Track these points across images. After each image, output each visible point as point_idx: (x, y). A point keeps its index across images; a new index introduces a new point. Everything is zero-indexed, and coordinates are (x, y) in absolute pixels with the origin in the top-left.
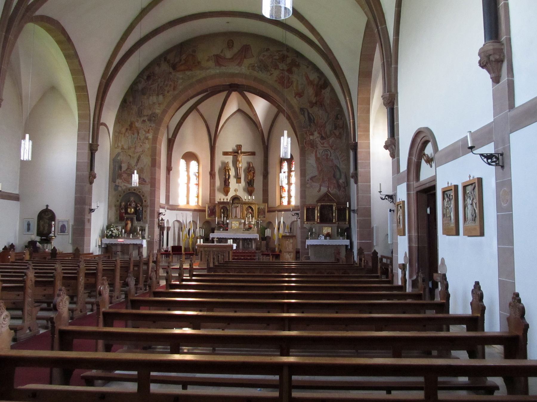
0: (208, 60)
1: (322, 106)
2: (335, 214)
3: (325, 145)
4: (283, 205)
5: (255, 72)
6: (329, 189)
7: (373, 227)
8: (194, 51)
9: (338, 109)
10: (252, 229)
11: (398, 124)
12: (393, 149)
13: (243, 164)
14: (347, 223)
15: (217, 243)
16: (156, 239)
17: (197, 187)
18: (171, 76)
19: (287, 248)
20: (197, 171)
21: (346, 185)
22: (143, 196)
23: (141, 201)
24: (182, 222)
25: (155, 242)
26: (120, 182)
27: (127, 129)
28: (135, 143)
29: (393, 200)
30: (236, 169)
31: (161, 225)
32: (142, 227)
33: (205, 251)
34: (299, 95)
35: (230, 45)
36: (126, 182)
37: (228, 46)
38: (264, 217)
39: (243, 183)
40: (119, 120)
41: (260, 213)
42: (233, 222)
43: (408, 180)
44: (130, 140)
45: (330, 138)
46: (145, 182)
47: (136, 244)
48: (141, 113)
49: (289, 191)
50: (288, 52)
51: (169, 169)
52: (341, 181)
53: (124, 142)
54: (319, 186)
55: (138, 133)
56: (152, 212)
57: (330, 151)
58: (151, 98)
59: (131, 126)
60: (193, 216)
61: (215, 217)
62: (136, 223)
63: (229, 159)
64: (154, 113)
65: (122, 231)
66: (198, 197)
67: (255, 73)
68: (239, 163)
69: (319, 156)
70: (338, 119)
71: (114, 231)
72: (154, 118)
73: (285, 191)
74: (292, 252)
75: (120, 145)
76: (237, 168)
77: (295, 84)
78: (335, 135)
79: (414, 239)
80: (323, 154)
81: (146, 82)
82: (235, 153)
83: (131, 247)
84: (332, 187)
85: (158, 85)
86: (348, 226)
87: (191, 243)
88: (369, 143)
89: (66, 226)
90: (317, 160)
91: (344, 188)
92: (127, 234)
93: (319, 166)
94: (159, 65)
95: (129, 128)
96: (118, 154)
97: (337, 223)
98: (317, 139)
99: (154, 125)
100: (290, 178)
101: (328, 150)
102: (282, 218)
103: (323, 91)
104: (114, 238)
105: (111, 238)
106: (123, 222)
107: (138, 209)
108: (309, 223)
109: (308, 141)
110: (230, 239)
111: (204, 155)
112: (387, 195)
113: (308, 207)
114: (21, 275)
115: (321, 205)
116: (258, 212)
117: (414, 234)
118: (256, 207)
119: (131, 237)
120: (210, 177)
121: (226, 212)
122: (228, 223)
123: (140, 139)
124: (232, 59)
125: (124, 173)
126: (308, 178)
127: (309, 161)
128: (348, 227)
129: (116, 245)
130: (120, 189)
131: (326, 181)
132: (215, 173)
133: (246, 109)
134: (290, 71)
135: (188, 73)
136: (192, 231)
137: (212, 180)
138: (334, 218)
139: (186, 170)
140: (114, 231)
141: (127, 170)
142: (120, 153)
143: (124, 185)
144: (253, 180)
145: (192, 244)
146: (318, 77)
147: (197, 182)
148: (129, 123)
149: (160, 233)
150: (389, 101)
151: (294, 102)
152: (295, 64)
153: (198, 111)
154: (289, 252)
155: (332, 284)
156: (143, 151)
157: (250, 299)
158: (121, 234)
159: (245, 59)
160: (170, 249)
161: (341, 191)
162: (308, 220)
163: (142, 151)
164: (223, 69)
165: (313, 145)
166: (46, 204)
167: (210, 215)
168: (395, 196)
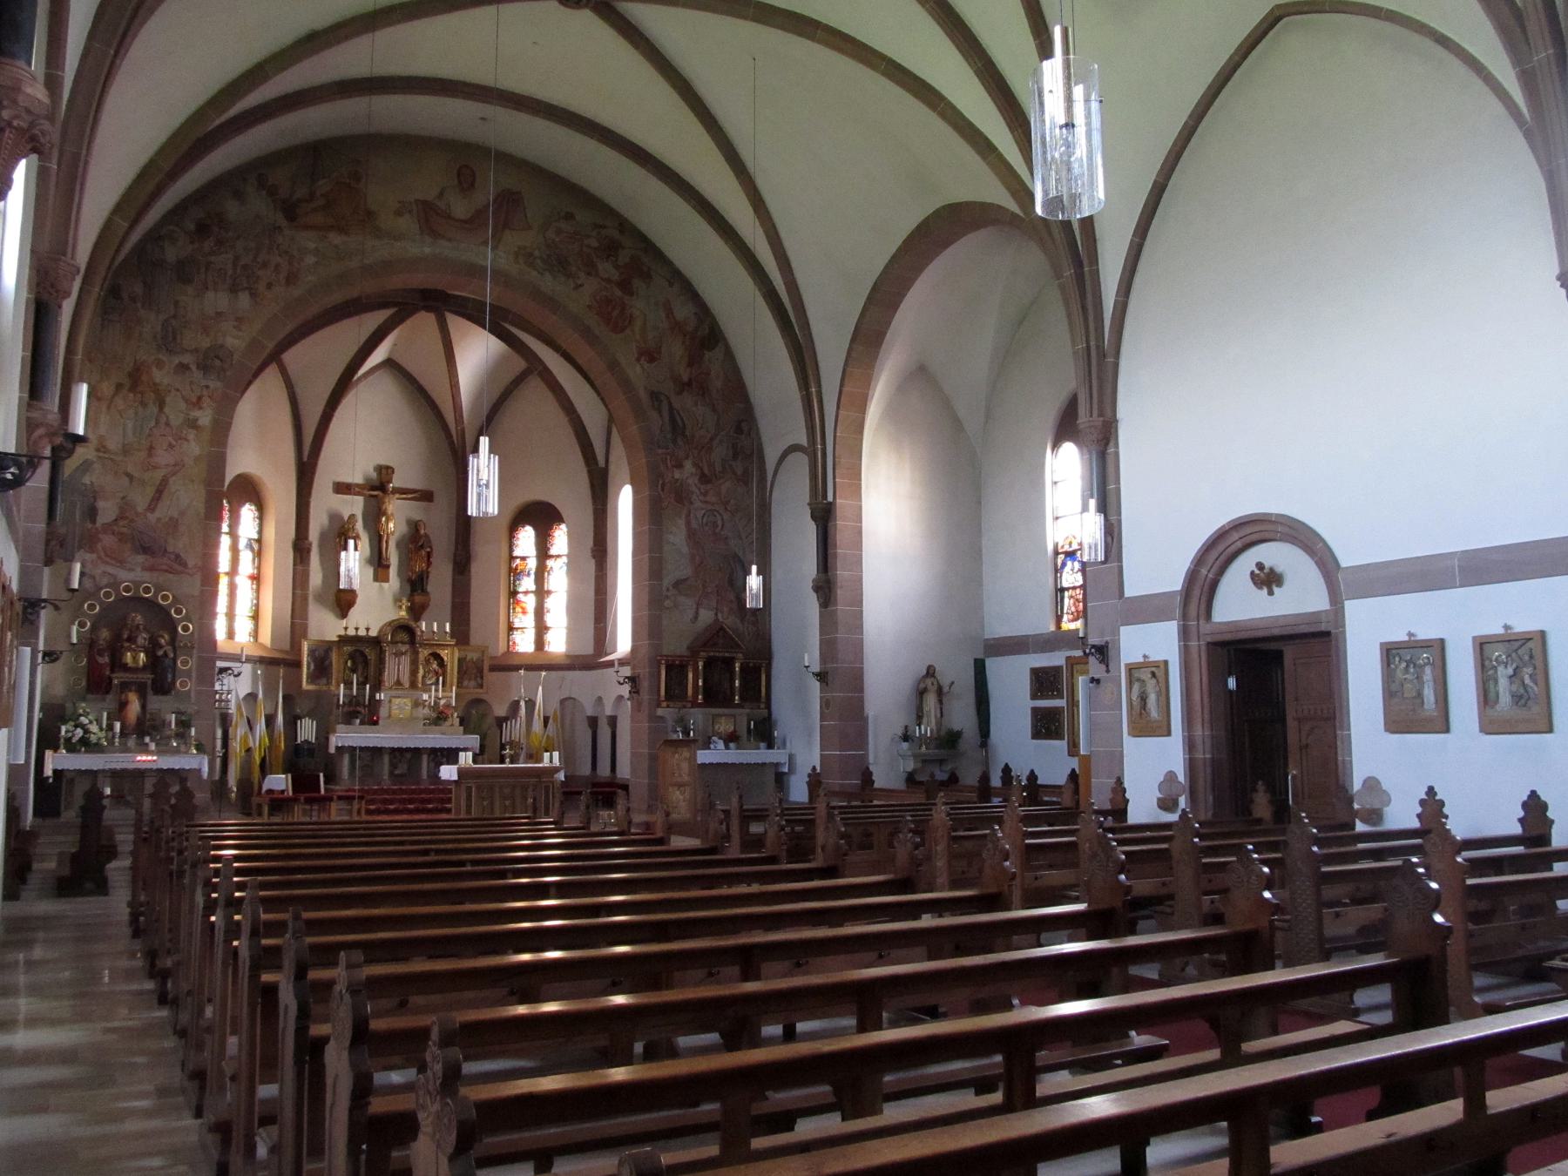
0: (399, 213)
1: (703, 394)
4: (517, 653)
5: (534, 273)
6: (720, 615)
13: (394, 527)
14: (763, 706)
17: (254, 586)
20: (256, 536)
23: (171, 626)
27: (119, 387)
28: (149, 435)
33: (479, 788)
34: (650, 355)
35: (466, 181)
36: (113, 562)
38: (481, 686)
39: (394, 582)
43: (1185, 616)
44: (130, 425)
45: (721, 481)
46: (185, 565)
48: (175, 338)
49: (540, 612)
54: (695, 606)
55: (161, 405)
57: (720, 514)
58: (210, 295)
63: (354, 506)
64: (222, 346)
65: (110, 727)
71: (94, 728)
72: (217, 362)
73: (524, 612)
76: (380, 537)
77: (638, 324)
80: (705, 520)
81: (192, 243)
82: (373, 488)
85: (237, 258)
88: (860, 508)
98: (690, 481)
99: (219, 384)
102: (540, 688)
103: (708, 355)
106: (109, 697)
108: (671, 704)
110: (465, 750)
118: (453, 654)
120: (295, 558)
122: (380, 700)
123: (167, 424)
126: (666, 582)
127: (671, 538)
132: (311, 544)
134: (625, 285)
135: (336, 239)
137: (299, 568)
138: (701, 690)
141: (116, 520)
142: (93, 463)
144: (428, 573)
146: (696, 314)
150: (1100, 437)
154: (680, 786)
155: (436, 882)
156: (178, 466)
162: (670, 696)
164: (445, 249)
167: (313, 678)
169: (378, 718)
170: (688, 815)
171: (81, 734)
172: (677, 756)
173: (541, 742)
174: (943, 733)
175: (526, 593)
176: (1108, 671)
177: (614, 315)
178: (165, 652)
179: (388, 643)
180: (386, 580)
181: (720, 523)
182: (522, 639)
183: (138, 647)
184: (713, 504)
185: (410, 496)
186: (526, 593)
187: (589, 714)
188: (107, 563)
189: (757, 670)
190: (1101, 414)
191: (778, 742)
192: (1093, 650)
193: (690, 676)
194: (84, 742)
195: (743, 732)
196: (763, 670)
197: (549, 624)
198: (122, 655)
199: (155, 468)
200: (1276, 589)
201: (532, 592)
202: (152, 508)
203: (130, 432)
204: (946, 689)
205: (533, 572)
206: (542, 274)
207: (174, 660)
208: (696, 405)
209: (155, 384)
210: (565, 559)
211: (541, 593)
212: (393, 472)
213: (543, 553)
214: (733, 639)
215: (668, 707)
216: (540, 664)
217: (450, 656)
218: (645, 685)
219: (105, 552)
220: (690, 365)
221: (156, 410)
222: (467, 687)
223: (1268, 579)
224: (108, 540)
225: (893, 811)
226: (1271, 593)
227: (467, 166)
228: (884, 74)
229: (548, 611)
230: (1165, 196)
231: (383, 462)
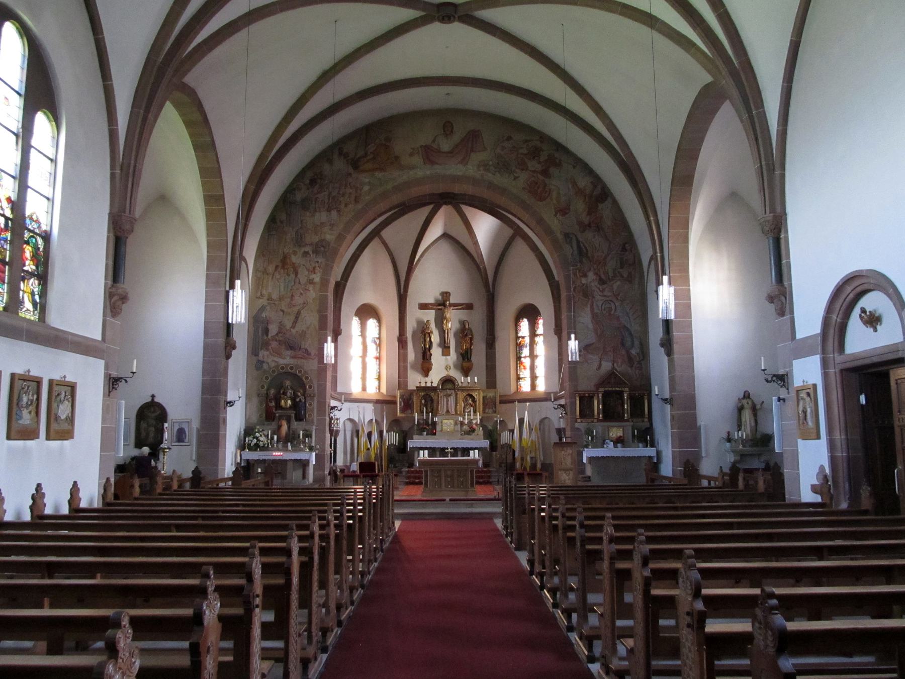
0: (411, 155)
2: (628, 406)
3: (606, 293)
4: (522, 392)
5: (490, 175)
6: (615, 365)
7: (700, 426)
8: (388, 139)
10: (476, 432)
11: (789, 264)
12: (783, 303)
13: (452, 326)
14: (646, 420)
15: (451, 457)
17: (378, 363)
18: (350, 180)
19: (563, 464)
20: (378, 336)
21: (641, 358)
22: (307, 378)
23: (303, 386)
24: (357, 421)
27: (277, 267)
28: (291, 290)
29: (784, 382)
30: (442, 332)
32: (307, 431)
33: (432, 471)
34: (563, 211)
37: (444, 131)
39: (453, 356)
40: (263, 250)
41: (487, 405)
42: (445, 421)
43: (824, 351)
46: (309, 354)
50: (542, 142)
52: (634, 352)
53: (275, 288)
55: (296, 274)
58: (317, 214)
59: (284, 262)
60: (375, 411)
61: (412, 413)
62: (295, 424)
63: (430, 315)
64: (324, 240)
65: (272, 438)
66: (379, 379)
67: (489, 176)
68: (448, 322)
69: (596, 311)
70: (626, 250)
71: (262, 439)
72: (322, 249)
73: (525, 368)
74: (571, 470)
75: (264, 292)
76: (444, 331)
77: (554, 195)
78: (622, 276)
79: (839, 444)
80: (603, 308)
81: (308, 189)
83: (290, 466)
84: (620, 361)
85: (330, 193)
89: (186, 430)
91: (639, 362)
94: (330, 161)
95: (280, 264)
96: (263, 308)
97: (630, 420)
98: (593, 284)
100: (533, 346)
102: (526, 412)
103: (601, 206)
104: (260, 450)
105: (256, 450)
106: (273, 423)
107: (298, 400)
111: (390, 311)
112: (774, 376)
113: (582, 395)
114: (194, 516)
115: (605, 392)
116: (483, 404)
117: (839, 436)
118: (479, 395)
119: (290, 448)
121: (429, 403)
123: (299, 283)
124: (451, 153)
125: (273, 340)
128: (648, 426)
130: (265, 366)
131: (610, 351)
132: (407, 338)
133: (459, 232)
134: (545, 173)
135: (379, 175)
136: (375, 436)
138: (601, 411)
139: (360, 334)
141: (277, 334)
144: (471, 350)
145: (375, 457)
146: (592, 182)
147: (378, 355)
150: (773, 227)
151: (555, 223)
152: (552, 162)
153: (381, 238)
154: (566, 470)
156: (305, 303)
157: (34, 561)
158: (271, 443)
159: (472, 154)
161: (634, 368)
162: (583, 415)
164: (438, 169)
165: (586, 293)
166: (151, 394)
167: (403, 410)
168: (787, 375)
172: (563, 452)
173: (527, 444)
174: (759, 436)
175: (525, 357)
176: (789, 393)
177: (539, 191)
179: (440, 389)
180: (449, 354)
181: (613, 308)
184: (608, 297)
185: (460, 307)
186: (525, 357)
187: (556, 427)
189: (642, 398)
190: (773, 210)
192: (774, 378)
194: (257, 445)
196: (646, 397)
197: (537, 375)
198: (280, 401)
200: (878, 327)
202: (293, 327)
203: (282, 289)
204: (758, 407)
205: (528, 345)
206: (494, 175)
207: (305, 402)
208: (594, 237)
209: (294, 264)
211: (533, 356)
213: (533, 334)
214: (621, 379)
215: (582, 422)
216: (534, 399)
217: (479, 396)
220: (589, 214)
223: (872, 320)
224: (274, 344)
225: (267, 492)
226: (875, 330)
227: (449, 122)
228: (621, 14)
230: (801, 49)
231: (445, 290)
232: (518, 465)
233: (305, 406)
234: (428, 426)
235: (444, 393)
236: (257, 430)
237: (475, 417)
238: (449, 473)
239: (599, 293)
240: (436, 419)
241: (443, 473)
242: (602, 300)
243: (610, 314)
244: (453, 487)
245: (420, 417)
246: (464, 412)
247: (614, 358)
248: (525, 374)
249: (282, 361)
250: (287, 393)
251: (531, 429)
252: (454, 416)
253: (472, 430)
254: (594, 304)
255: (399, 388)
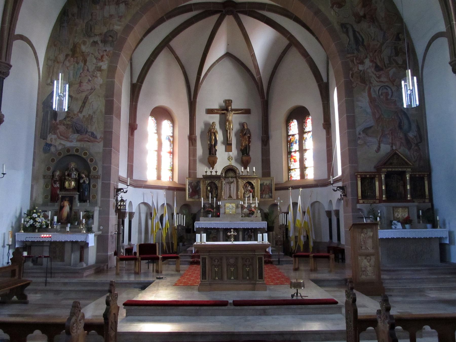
3: (383, 79)
9: (399, 25)
10: (255, 215)
14: (427, 201)
16: (112, 232)
17: (171, 157)
20: (171, 135)
22: (92, 160)
24: (151, 204)
25: (109, 236)
26: (54, 138)
27: (67, 56)
28: (80, 77)
31: (120, 209)
33: (211, 258)
38: (271, 197)
39: (234, 152)
41: (264, 191)
42: (227, 205)
45: (389, 69)
46: (96, 138)
47: (77, 242)
49: (302, 160)
51: (133, 127)
55: (85, 61)
56: (106, 187)
58: (107, 7)
59: (74, 50)
60: (167, 197)
61: (200, 198)
63: (215, 119)
64: (112, 30)
65: (52, 219)
66: (172, 170)
70: (400, 40)
72: (111, 39)
73: (295, 161)
76: (227, 131)
78: (397, 63)
83: (68, 248)
84: (398, 143)
86: (429, 205)
87: (164, 235)
90: (371, 102)
92: (62, 224)
93: (375, 111)
95: (70, 53)
98: (369, 71)
101: (387, 86)
102: (300, 197)
104: (39, 231)
105: (34, 231)
106: (56, 204)
107: (82, 181)
108: (366, 201)
109: (356, 72)
113: (363, 176)
119: (68, 229)
122: (220, 205)
123: (88, 70)
125: (60, 125)
126: (359, 129)
129: (41, 244)
130: (53, 149)
132: (196, 137)
136: (166, 218)
138: (384, 192)
139: (156, 132)
140: (37, 219)
141: (65, 118)
143: (60, 144)
144: (249, 146)
145: (166, 237)
147: (172, 150)
148: (71, 46)
149: (119, 222)
153: (172, 51)
154: (367, 255)
156: (93, 89)
160: (136, 249)
162: (364, 196)
163: (92, 89)
167: (191, 196)
168: (346, 187)
169: (220, 214)
170: (374, 277)
171: (32, 223)
172: (363, 235)
173: (301, 225)
175: (295, 152)
178: (84, 181)
182: (295, 174)
183: (72, 179)
184: (384, 82)
185: (240, 112)
186: (295, 152)
187: (327, 210)
188: (61, 139)
189: (422, 179)
191: (440, 223)
193: (377, 184)
195: (414, 218)
196: (426, 179)
197: (306, 166)
199: (82, 92)
201: (298, 151)
202: (81, 112)
205: (297, 141)
209: (83, 52)
210: (311, 134)
211: (302, 150)
212: (232, 102)
213: (302, 132)
215: (364, 203)
217: (257, 184)
218: (349, 190)
219: (60, 133)
220: (364, 6)
221: (83, 65)
222: (265, 198)
224: (62, 128)
229: (306, 160)
232: (292, 243)
233: (90, 187)
234: (213, 210)
235: (227, 180)
236: (35, 211)
237: (254, 202)
238: (232, 261)
239: (376, 79)
240: (220, 203)
241: (224, 261)
242: (378, 86)
243: (387, 99)
244: (236, 278)
245: (206, 202)
246: (244, 197)
247: (392, 140)
248: (296, 165)
249: (68, 144)
250: (71, 174)
251: (304, 213)
252: (236, 201)
253: (251, 213)
254: (372, 89)
255: (190, 176)
